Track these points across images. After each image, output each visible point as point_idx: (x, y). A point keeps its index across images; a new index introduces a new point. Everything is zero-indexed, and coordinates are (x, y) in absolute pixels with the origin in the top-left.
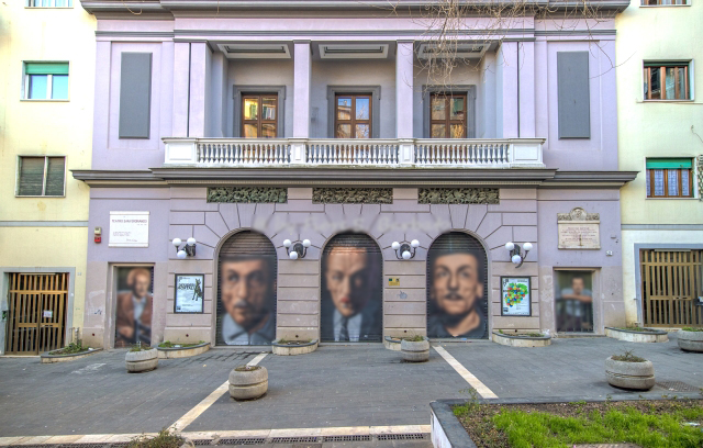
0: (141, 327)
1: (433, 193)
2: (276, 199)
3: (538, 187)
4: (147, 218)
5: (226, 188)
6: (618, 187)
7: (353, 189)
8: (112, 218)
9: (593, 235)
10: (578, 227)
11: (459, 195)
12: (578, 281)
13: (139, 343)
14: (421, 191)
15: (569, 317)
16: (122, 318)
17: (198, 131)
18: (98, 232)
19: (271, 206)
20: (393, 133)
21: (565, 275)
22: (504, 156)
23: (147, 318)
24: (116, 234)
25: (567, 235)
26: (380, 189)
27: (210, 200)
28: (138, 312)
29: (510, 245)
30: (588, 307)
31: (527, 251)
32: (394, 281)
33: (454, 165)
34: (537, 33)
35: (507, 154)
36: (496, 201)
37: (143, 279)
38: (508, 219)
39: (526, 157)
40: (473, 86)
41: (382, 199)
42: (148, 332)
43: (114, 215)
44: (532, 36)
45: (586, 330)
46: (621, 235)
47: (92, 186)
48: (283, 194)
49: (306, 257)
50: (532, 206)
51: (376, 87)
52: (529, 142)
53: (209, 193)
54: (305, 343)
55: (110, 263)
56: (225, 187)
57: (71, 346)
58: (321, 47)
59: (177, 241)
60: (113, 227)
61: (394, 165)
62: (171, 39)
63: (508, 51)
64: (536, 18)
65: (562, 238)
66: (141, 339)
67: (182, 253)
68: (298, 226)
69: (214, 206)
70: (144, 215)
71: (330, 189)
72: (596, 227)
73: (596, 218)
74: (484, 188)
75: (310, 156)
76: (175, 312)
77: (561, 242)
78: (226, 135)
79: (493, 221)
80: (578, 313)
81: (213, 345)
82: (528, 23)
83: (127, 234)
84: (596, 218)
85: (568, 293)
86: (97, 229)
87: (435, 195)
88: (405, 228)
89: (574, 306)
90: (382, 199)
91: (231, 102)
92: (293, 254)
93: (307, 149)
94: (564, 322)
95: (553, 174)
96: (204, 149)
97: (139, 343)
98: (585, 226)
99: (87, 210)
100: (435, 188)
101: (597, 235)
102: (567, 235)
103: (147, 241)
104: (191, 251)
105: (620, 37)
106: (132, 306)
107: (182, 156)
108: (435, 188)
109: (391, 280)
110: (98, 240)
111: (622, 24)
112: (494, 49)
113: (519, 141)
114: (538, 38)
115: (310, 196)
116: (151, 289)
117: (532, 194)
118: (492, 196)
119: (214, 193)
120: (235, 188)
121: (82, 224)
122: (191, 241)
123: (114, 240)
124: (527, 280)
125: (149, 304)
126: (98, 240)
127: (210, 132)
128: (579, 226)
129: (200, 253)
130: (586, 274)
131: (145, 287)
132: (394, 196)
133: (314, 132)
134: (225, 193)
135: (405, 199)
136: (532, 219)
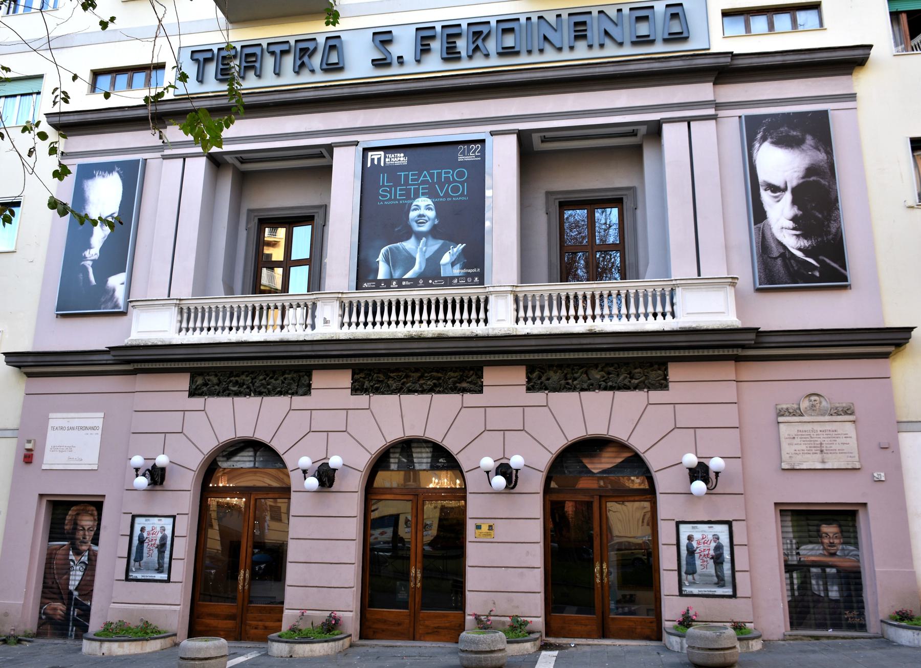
0: (78, 604)
1: (551, 373)
2: (294, 386)
3: (738, 359)
4: (99, 423)
5: (217, 372)
6: (886, 356)
7: (417, 370)
8: (52, 423)
9: (845, 442)
10: (821, 428)
11: (597, 375)
12: (829, 530)
13: (72, 630)
14: (529, 372)
15: (818, 599)
16: (52, 585)
17: (184, 289)
18: (29, 446)
19: (284, 400)
20: (665, 270)
21: (804, 520)
22: (482, 315)
23: (87, 587)
24: (54, 449)
25: (796, 442)
26: (297, 369)
27: (193, 393)
28: (76, 577)
29: (691, 459)
30: (852, 580)
31: (717, 474)
32: (485, 528)
33: (580, 327)
34: (718, 106)
35: (672, 305)
36: (663, 385)
37: (87, 522)
38: (687, 416)
39: (706, 309)
40: (632, 189)
41: (464, 385)
42: (86, 613)
43: (56, 420)
44: (711, 112)
45: (851, 627)
46: (897, 438)
47: (29, 375)
48: (305, 380)
49: (517, 489)
50: (728, 392)
51: (320, 207)
52: (715, 283)
53: (192, 381)
54: (146, 632)
55: (41, 496)
56: (216, 371)
57: (293, 629)
58: (536, 138)
59: (137, 460)
60: (53, 438)
61: (668, 324)
62: (158, 155)
63: (673, 135)
64: (714, 84)
65: (786, 449)
66: (76, 623)
67: (142, 482)
68: (331, 433)
69: (198, 402)
70: (96, 419)
71: (379, 371)
72: (849, 429)
73: (848, 411)
74: (639, 363)
75: (522, 314)
76: (127, 579)
77: (785, 456)
78: (551, 280)
79: (298, 422)
80: (834, 593)
81: (355, 638)
82: (704, 91)
83: (70, 449)
84: (848, 411)
85: (811, 552)
86: (29, 442)
87: (555, 377)
88: (505, 438)
89: (824, 577)
90: (464, 385)
91: (243, 234)
92: (499, 481)
93: (517, 301)
94: (803, 611)
95: (752, 336)
96: (187, 314)
97: (72, 630)
98: (828, 427)
99: (19, 412)
100: (556, 365)
101: (853, 442)
102: (796, 442)
103: (95, 459)
104: (157, 476)
105: (862, 102)
106: (67, 570)
107: (155, 327)
108: (556, 365)
109: (478, 527)
110: (28, 458)
111: (862, 83)
112: (655, 131)
113: (700, 281)
114: (721, 113)
115: (523, 380)
116: (95, 541)
117: (727, 370)
118: (654, 375)
119: (200, 381)
120: (232, 372)
121: (9, 434)
122: (162, 460)
123: (50, 459)
124: (725, 528)
125: (90, 567)
126: (28, 458)
127: (201, 286)
128: (817, 427)
129: (170, 481)
130: (846, 517)
131: (89, 536)
132: (486, 381)
133: (525, 276)
134: (215, 380)
135: (332, 390)
136: (729, 415)
